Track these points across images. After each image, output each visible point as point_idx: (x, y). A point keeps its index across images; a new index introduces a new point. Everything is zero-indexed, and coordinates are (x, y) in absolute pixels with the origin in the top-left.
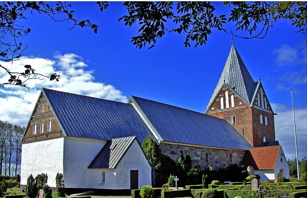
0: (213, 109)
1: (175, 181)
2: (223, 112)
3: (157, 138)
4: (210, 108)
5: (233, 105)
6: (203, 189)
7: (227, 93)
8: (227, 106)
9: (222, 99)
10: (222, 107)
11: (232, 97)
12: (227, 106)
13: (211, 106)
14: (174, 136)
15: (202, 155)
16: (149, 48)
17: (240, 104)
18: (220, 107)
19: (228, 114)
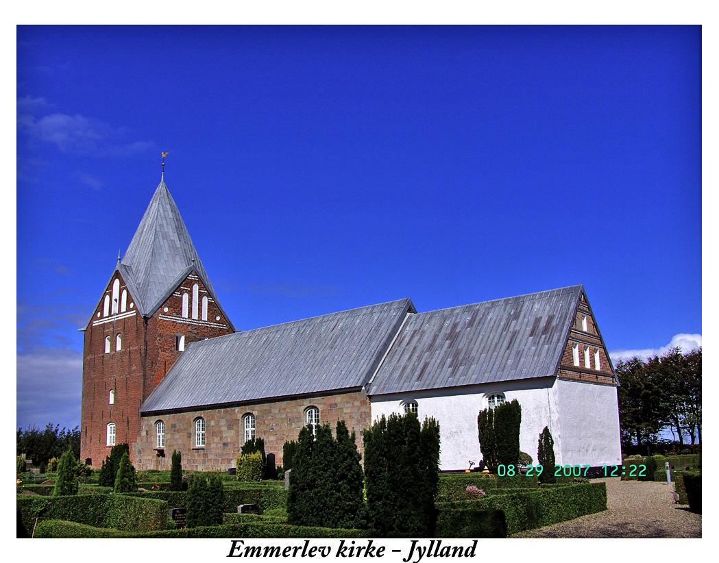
0: (166, 310)
1: (672, 481)
2: (186, 324)
3: (118, 474)
4: (161, 307)
5: (205, 317)
6: (339, 529)
7: (196, 288)
8: (195, 316)
9: (186, 297)
10: (185, 313)
11: (205, 300)
12: (195, 316)
13: (164, 303)
14: (267, 486)
15: (307, 498)
16: (400, 551)
17: (218, 318)
18: (180, 313)
19: (196, 331)
